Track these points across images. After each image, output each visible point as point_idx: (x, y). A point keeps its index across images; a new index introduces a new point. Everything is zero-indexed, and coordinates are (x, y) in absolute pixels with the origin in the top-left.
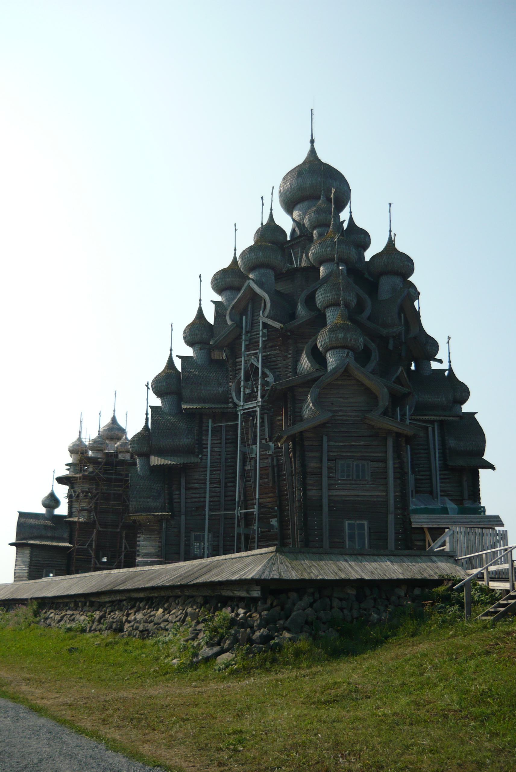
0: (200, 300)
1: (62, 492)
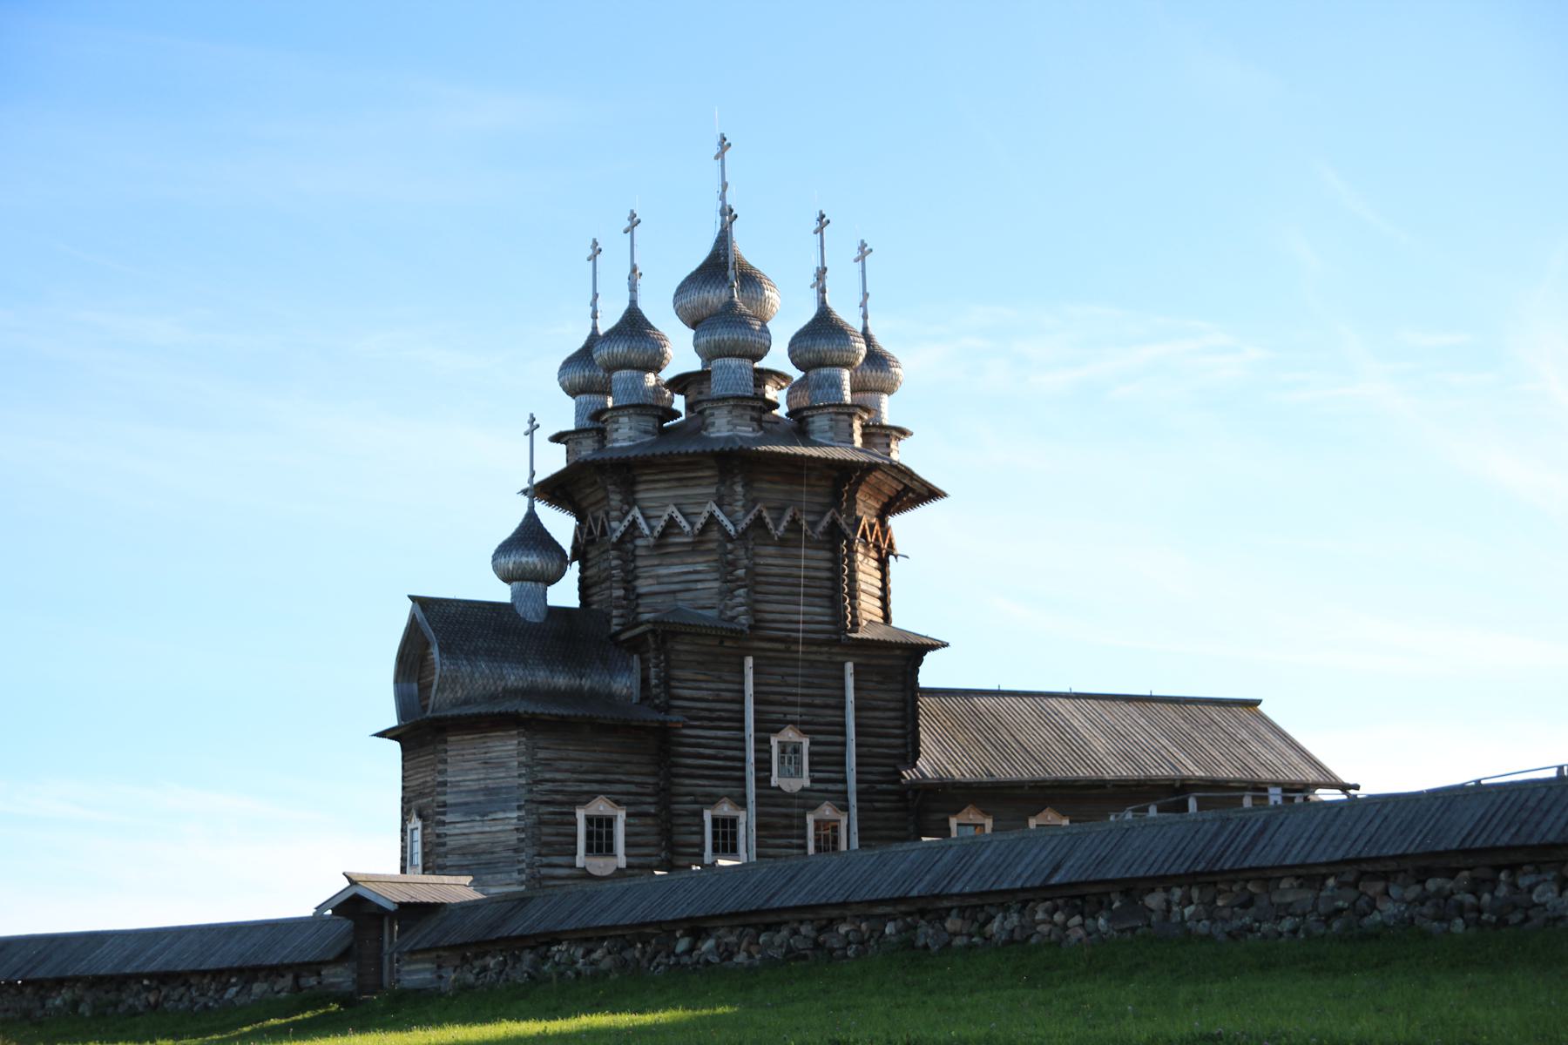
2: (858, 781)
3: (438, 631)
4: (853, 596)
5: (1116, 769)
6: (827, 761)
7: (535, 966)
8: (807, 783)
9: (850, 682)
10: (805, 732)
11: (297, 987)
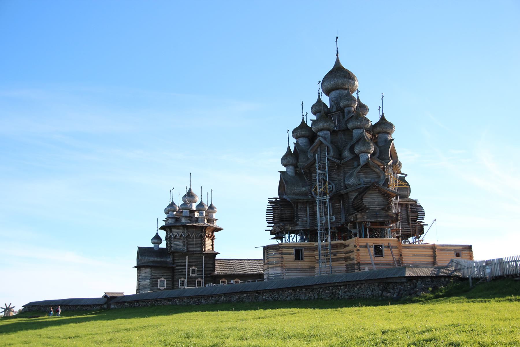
1: (163, 234)
3: (142, 252)
4: (205, 246)
5: (249, 272)
7: (405, 282)
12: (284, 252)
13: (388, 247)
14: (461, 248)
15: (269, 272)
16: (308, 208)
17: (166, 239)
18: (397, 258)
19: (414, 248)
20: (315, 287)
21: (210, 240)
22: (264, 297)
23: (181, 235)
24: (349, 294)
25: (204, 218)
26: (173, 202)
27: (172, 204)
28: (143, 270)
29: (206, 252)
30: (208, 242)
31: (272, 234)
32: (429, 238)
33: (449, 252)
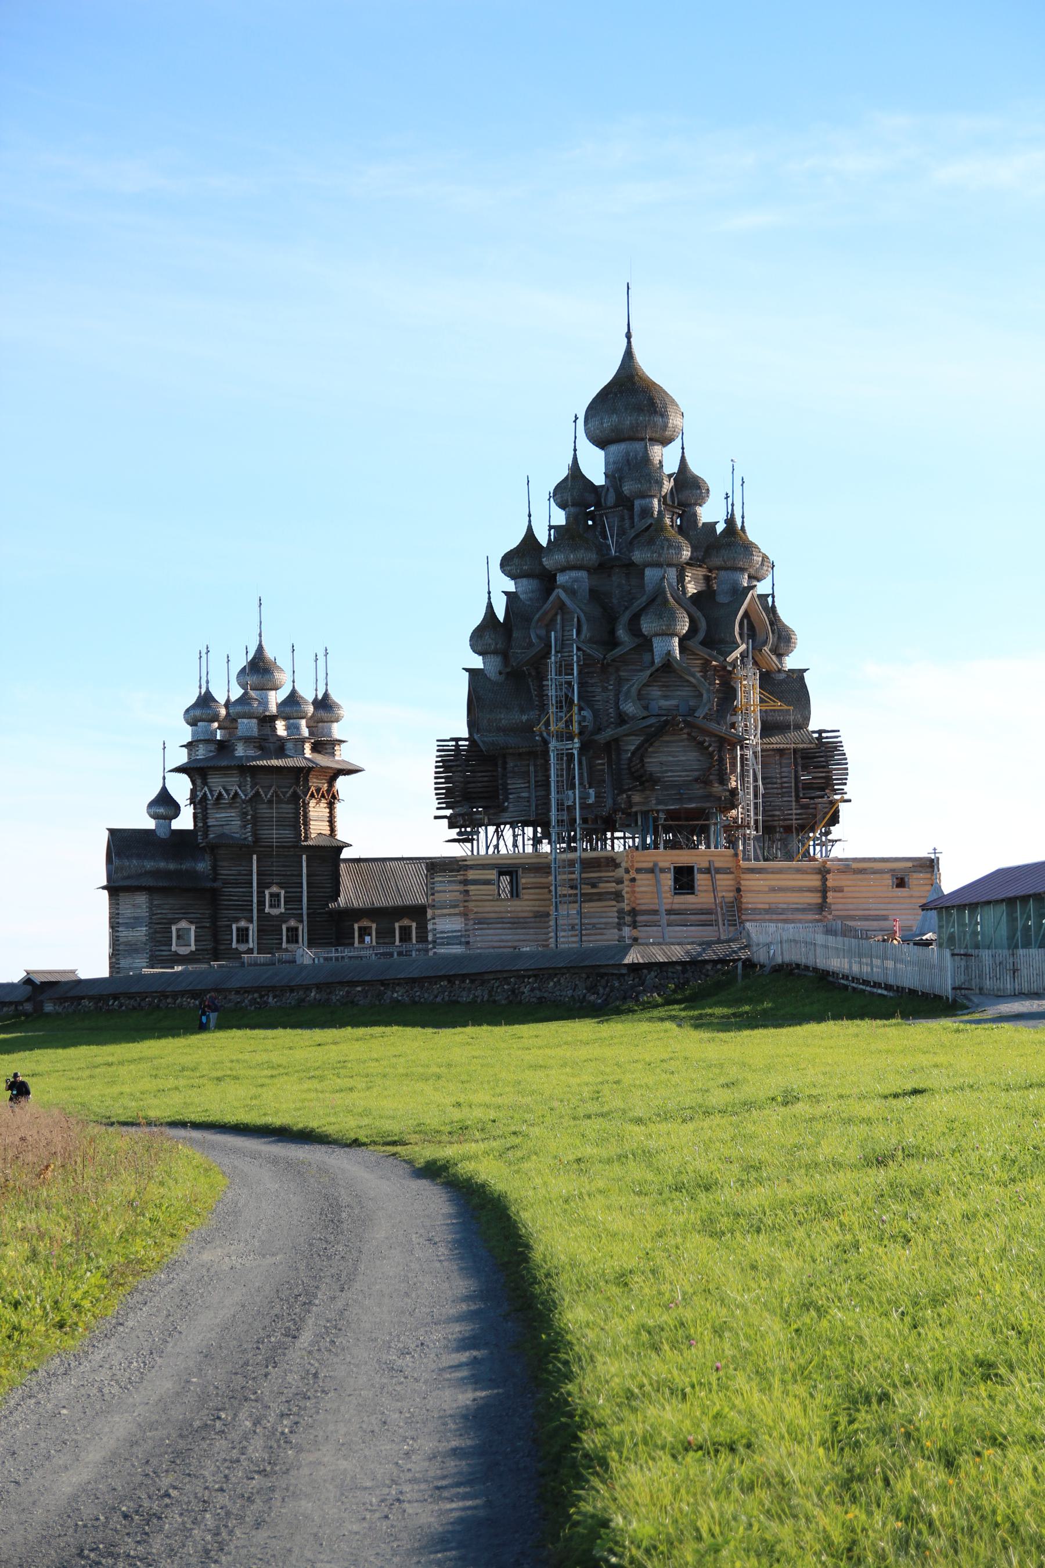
0: (489, 593)
1: (181, 788)
2: (308, 909)
3: (122, 844)
4: (306, 824)
6: (293, 900)
8: (283, 910)
9: (304, 864)
10: (282, 888)
11: (16, 1009)
12: (470, 877)
13: (707, 871)
14: (910, 864)
15: (437, 927)
16: (532, 768)
17: (193, 800)
18: (730, 896)
19: (773, 873)
20: (486, 977)
21: (323, 804)
22: (395, 995)
23: (236, 794)
24: (538, 993)
25: (303, 741)
26: (208, 693)
27: (206, 700)
28: (125, 898)
29: (310, 843)
30: (317, 811)
31: (451, 826)
32: (865, 829)
33: (878, 876)
